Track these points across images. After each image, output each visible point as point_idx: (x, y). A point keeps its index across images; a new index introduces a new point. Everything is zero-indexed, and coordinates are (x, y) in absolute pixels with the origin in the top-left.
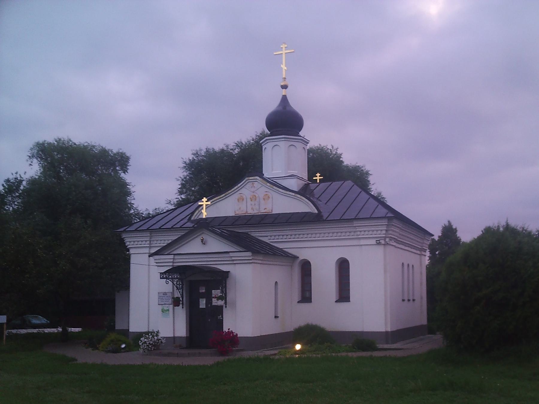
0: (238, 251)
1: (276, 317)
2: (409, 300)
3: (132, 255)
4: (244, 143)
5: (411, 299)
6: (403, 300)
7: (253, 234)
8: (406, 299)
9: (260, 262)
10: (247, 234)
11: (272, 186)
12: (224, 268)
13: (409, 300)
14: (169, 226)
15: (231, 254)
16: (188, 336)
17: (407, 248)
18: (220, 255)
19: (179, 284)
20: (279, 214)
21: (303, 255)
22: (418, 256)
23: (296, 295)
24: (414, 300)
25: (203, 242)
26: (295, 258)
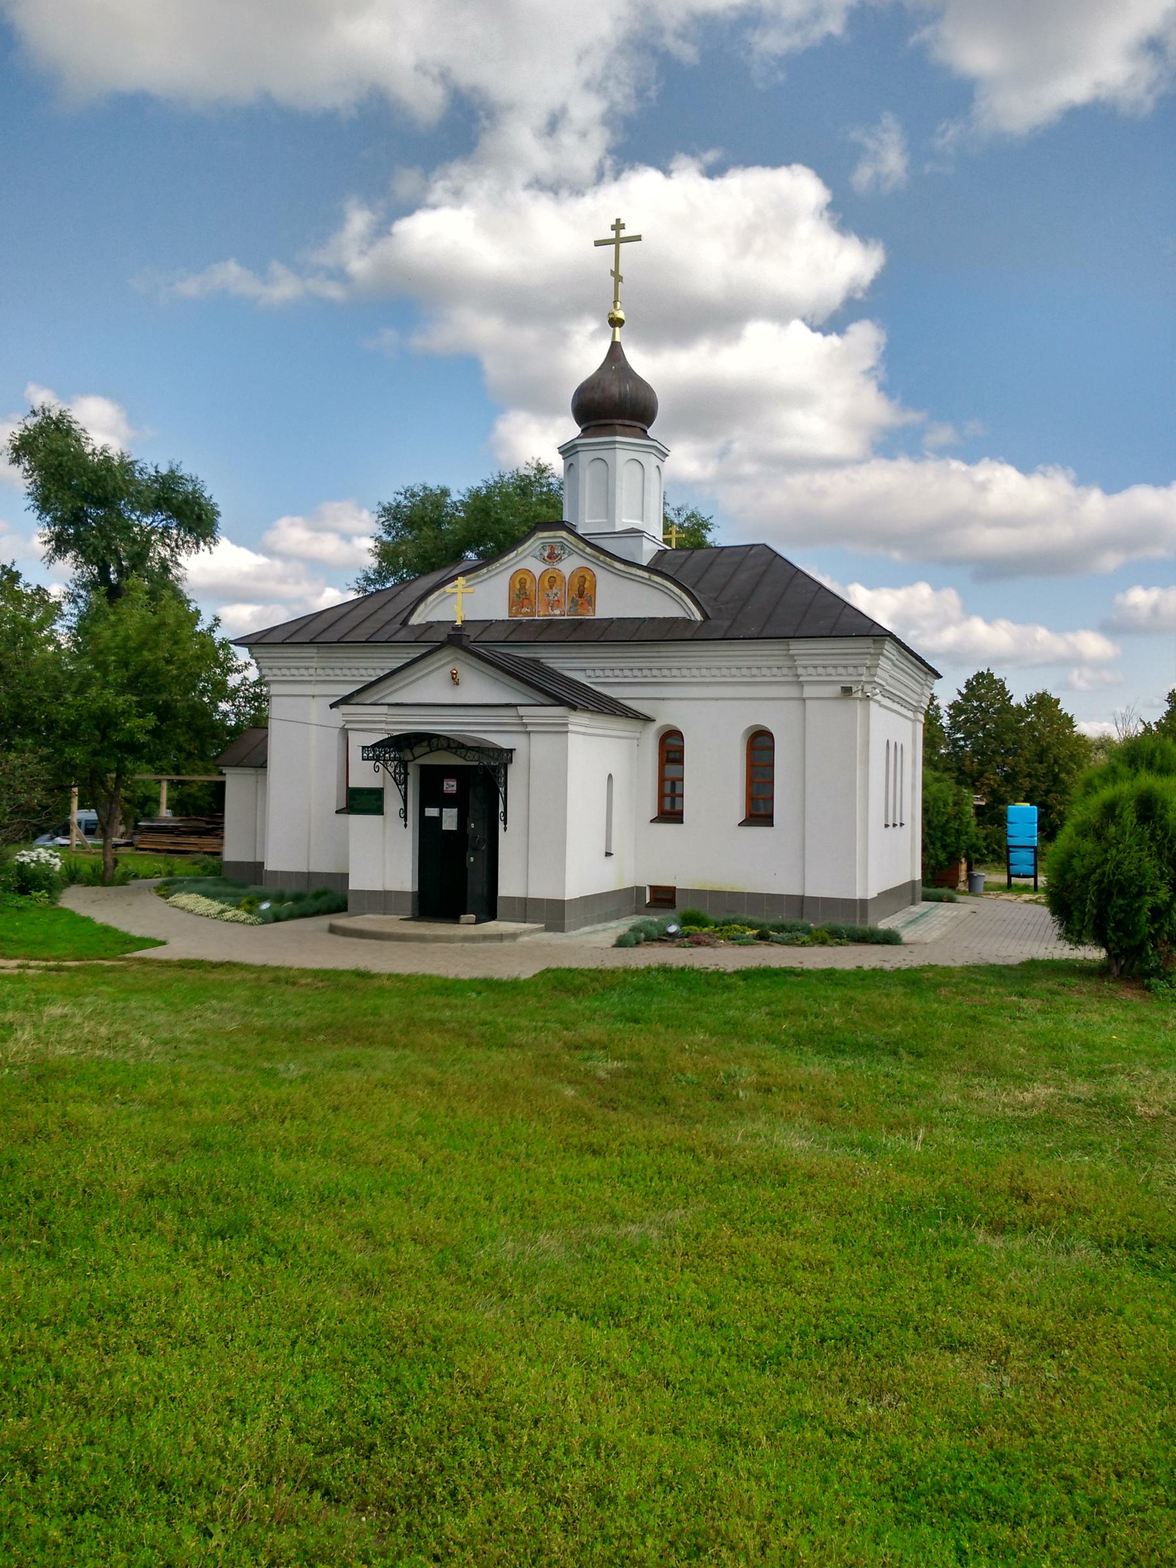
0: (533, 702)
1: (608, 854)
2: (895, 825)
3: (273, 699)
4: (1059, 707)
5: (898, 823)
6: (887, 826)
7: (554, 664)
8: (891, 824)
9: (583, 729)
10: (536, 661)
11: (597, 554)
12: (503, 742)
13: (895, 825)
14: (361, 634)
15: (522, 711)
16: (416, 889)
17: (896, 707)
18: (471, 711)
19: (400, 774)
20: (611, 621)
21: (668, 715)
22: (910, 723)
23: (737, 807)
24: (902, 825)
25: (455, 680)
26: (648, 719)
